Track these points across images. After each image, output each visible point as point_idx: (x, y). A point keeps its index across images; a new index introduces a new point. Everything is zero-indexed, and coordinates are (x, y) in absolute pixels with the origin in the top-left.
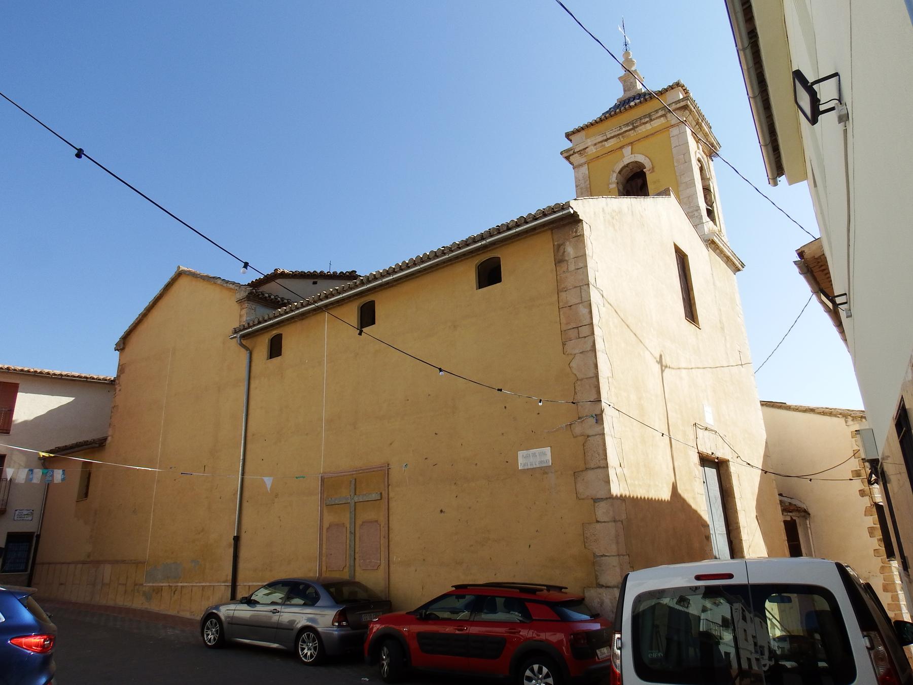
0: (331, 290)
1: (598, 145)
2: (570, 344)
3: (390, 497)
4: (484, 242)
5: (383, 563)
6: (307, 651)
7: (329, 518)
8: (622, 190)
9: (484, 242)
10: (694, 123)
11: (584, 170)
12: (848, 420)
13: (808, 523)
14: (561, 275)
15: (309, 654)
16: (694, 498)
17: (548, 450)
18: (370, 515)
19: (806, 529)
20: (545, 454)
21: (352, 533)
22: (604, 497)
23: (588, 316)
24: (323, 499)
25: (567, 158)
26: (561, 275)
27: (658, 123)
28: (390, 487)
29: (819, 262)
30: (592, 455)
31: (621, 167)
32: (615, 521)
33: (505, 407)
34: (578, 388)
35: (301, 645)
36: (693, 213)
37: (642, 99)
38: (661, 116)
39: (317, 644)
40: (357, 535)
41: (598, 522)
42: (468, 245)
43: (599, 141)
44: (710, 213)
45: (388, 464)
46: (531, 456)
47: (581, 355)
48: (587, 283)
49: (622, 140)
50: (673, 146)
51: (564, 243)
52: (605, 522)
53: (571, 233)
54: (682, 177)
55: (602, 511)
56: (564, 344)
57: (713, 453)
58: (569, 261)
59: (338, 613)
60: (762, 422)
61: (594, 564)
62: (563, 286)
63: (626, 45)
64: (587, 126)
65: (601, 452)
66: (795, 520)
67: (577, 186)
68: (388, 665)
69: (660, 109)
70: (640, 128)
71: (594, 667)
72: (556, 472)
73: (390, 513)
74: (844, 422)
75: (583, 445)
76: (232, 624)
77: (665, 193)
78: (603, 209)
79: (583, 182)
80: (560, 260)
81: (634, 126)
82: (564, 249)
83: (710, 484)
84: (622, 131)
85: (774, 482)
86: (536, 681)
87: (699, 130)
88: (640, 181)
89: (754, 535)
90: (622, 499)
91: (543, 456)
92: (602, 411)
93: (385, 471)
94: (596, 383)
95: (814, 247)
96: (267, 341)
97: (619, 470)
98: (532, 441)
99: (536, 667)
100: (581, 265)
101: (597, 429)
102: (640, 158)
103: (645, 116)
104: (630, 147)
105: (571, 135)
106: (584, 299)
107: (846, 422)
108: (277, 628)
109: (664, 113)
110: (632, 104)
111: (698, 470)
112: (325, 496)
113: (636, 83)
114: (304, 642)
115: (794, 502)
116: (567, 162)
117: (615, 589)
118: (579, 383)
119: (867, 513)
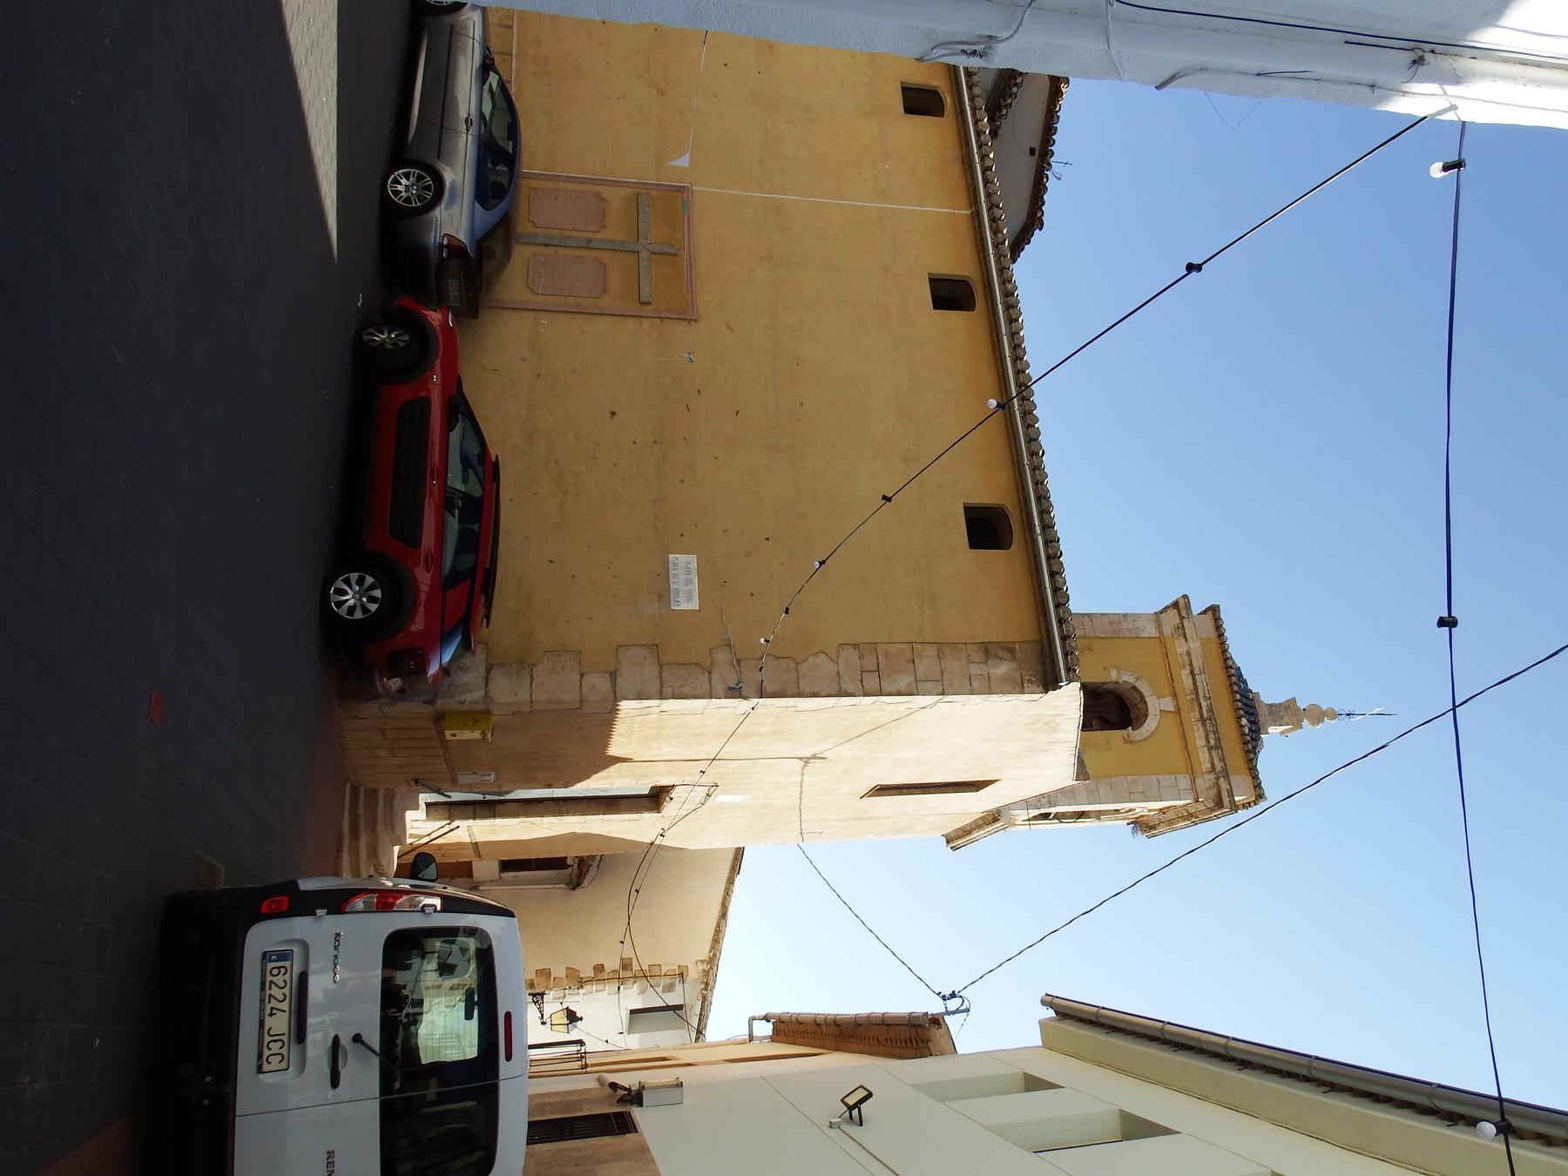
0: (1005, 231)
1: (1187, 658)
2: (853, 655)
3: (644, 320)
4: (1038, 530)
5: (537, 300)
6: (403, 185)
7: (615, 197)
8: (1105, 687)
9: (1038, 530)
10: (1192, 810)
11: (1151, 631)
12: (705, 965)
14: (964, 651)
15: (400, 188)
16: (607, 777)
17: (694, 605)
18: (616, 282)
19: (553, 882)
20: (689, 599)
21: (589, 243)
22: (618, 688)
23: (893, 689)
24: (650, 189)
25: (1175, 605)
26: (964, 651)
27: (1203, 757)
28: (657, 321)
29: (923, 1042)
30: (681, 676)
31: (1143, 691)
32: (581, 701)
33: (768, 539)
34: (784, 663)
35: (414, 173)
37: (1248, 738)
38: (1213, 765)
39: (414, 205)
40: (584, 253)
41: (582, 675)
42: (1038, 499)
43: (1193, 662)
44: (1046, 816)
45: (696, 320)
46: (687, 576)
47: (834, 673)
48: (946, 691)
49: (1185, 701)
50: (1161, 777)
51: (1016, 660)
52: (581, 686)
53: (1030, 672)
54: (1105, 786)
55: (597, 684)
56: (855, 646)
57: (671, 799)
58: (985, 666)
59: (463, 246)
60: (714, 847)
61: (520, 662)
62: (947, 652)
63: (1348, 715)
64: (1223, 643)
65: (685, 690)
67: (1125, 615)
68: (383, 343)
69: (1225, 765)
70: (1202, 730)
71: (376, 674)
72: (660, 617)
73: (616, 319)
74: (701, 959)
75: (698, 664)
76: (451, 33)
77: (1082, 772)
78: (1063, 715)
79: (1131, 626)
80: (989, 651)
81: (1206, 720)
82: (1006, 660)
84: (1202, 701)
86: (358, 592)
87: (1180, 815)
88: (1113, 718)
90: (613, 711)
91: (687, 598)
92: (745, 698)
93: (686, 314)
94: (789, 693)
95: (944, 1042)
96: (935, 83)
97: (658, 710)
98: (711, 580)
99: (377, 593)
100: (975, 685)
101: (719, 687)
102: (1151, 724)
103: (1218, 740)
104: (1172, 709)
105: (1214, 615)
106: (921, 685)
107: (702, 961)
108: (442, 126)
109: (1218, 770)
110: (1244, 721)
112: (654, 193)
113: (1280, 725)
114: (419, 178)
116: (1168, 602)
117: (483, 692)
118: (793, 665)
119: (570, 971)
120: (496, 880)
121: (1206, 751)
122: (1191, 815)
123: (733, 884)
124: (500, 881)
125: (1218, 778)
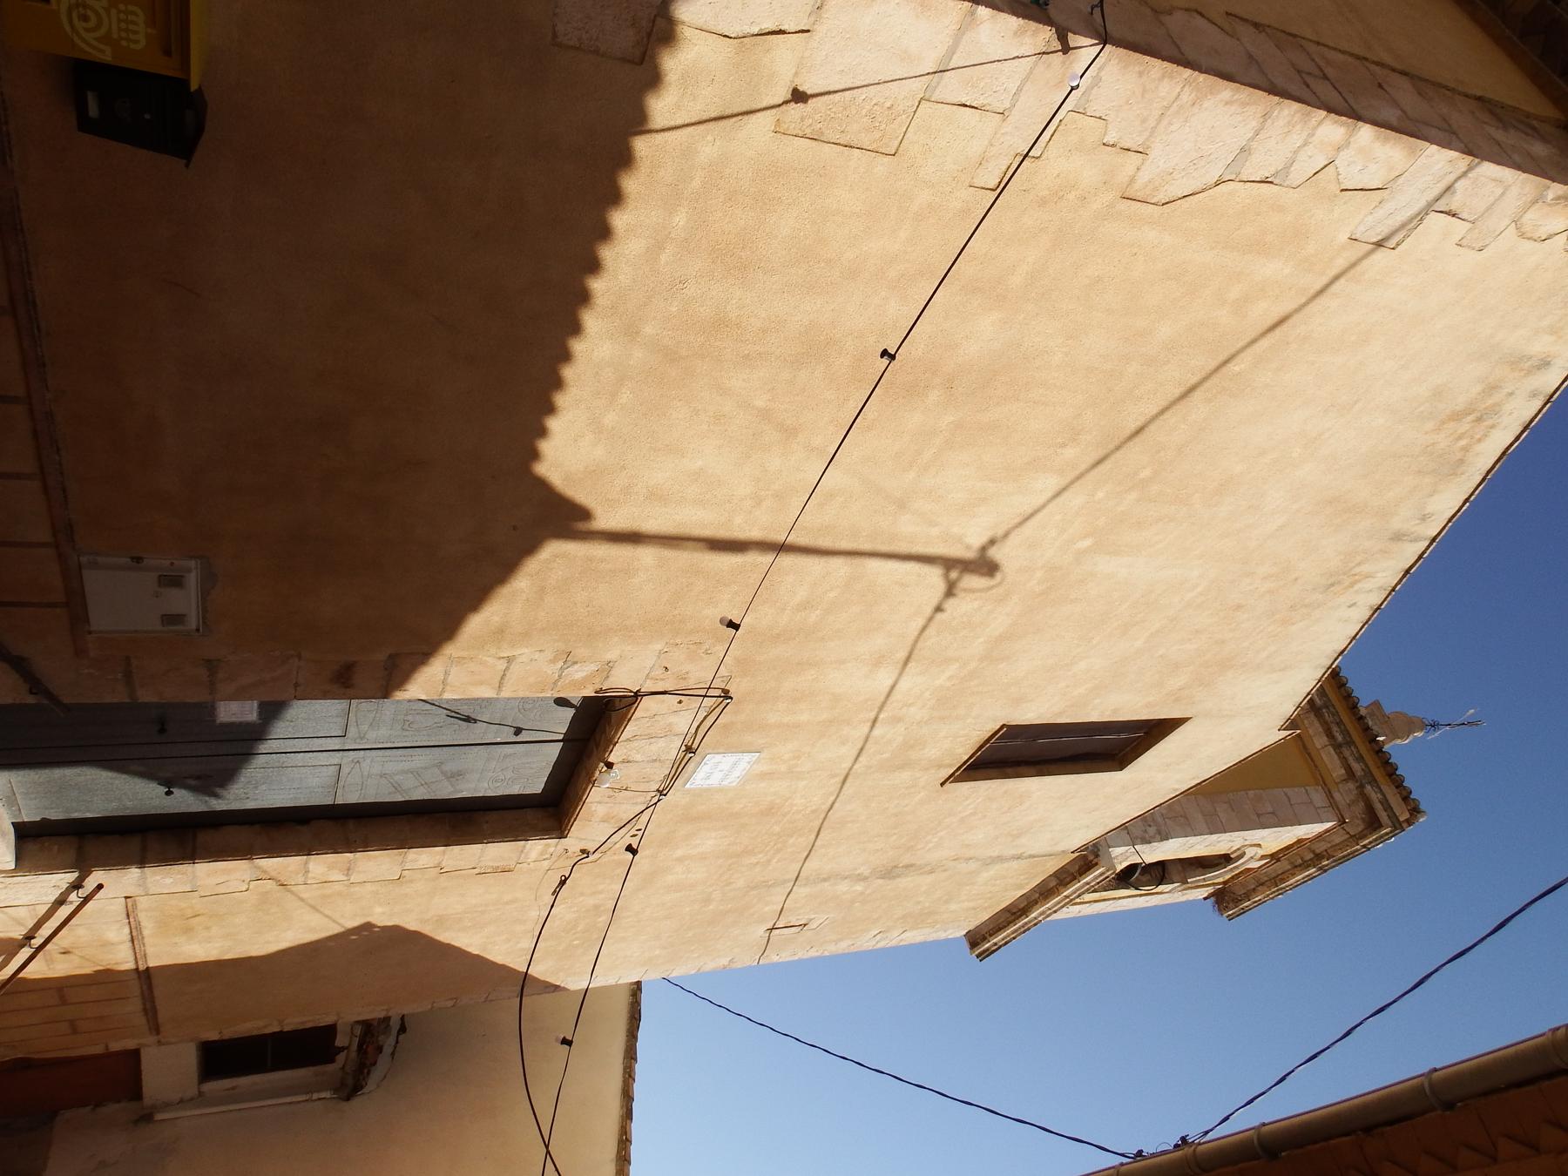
13: (323, 1095)
19: (307, 1089)
36: (1152, 824)
50: (1289, 791)
66: (332, 1061)
70: (1317, 724)
83: (506, 756)
85: (450, 1003)
89: (313, 907)
111: (582, 683)
115: (383, 1060)
120: (192, 1099)
121: (1332, 752)
122: (1319, 857)
123: (636, 1060)
124: (199, 1099)
125: (1362, 787)
